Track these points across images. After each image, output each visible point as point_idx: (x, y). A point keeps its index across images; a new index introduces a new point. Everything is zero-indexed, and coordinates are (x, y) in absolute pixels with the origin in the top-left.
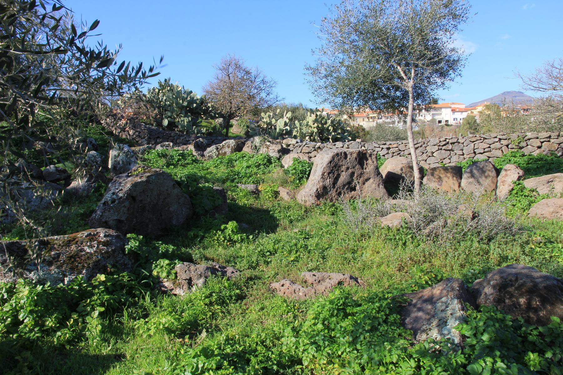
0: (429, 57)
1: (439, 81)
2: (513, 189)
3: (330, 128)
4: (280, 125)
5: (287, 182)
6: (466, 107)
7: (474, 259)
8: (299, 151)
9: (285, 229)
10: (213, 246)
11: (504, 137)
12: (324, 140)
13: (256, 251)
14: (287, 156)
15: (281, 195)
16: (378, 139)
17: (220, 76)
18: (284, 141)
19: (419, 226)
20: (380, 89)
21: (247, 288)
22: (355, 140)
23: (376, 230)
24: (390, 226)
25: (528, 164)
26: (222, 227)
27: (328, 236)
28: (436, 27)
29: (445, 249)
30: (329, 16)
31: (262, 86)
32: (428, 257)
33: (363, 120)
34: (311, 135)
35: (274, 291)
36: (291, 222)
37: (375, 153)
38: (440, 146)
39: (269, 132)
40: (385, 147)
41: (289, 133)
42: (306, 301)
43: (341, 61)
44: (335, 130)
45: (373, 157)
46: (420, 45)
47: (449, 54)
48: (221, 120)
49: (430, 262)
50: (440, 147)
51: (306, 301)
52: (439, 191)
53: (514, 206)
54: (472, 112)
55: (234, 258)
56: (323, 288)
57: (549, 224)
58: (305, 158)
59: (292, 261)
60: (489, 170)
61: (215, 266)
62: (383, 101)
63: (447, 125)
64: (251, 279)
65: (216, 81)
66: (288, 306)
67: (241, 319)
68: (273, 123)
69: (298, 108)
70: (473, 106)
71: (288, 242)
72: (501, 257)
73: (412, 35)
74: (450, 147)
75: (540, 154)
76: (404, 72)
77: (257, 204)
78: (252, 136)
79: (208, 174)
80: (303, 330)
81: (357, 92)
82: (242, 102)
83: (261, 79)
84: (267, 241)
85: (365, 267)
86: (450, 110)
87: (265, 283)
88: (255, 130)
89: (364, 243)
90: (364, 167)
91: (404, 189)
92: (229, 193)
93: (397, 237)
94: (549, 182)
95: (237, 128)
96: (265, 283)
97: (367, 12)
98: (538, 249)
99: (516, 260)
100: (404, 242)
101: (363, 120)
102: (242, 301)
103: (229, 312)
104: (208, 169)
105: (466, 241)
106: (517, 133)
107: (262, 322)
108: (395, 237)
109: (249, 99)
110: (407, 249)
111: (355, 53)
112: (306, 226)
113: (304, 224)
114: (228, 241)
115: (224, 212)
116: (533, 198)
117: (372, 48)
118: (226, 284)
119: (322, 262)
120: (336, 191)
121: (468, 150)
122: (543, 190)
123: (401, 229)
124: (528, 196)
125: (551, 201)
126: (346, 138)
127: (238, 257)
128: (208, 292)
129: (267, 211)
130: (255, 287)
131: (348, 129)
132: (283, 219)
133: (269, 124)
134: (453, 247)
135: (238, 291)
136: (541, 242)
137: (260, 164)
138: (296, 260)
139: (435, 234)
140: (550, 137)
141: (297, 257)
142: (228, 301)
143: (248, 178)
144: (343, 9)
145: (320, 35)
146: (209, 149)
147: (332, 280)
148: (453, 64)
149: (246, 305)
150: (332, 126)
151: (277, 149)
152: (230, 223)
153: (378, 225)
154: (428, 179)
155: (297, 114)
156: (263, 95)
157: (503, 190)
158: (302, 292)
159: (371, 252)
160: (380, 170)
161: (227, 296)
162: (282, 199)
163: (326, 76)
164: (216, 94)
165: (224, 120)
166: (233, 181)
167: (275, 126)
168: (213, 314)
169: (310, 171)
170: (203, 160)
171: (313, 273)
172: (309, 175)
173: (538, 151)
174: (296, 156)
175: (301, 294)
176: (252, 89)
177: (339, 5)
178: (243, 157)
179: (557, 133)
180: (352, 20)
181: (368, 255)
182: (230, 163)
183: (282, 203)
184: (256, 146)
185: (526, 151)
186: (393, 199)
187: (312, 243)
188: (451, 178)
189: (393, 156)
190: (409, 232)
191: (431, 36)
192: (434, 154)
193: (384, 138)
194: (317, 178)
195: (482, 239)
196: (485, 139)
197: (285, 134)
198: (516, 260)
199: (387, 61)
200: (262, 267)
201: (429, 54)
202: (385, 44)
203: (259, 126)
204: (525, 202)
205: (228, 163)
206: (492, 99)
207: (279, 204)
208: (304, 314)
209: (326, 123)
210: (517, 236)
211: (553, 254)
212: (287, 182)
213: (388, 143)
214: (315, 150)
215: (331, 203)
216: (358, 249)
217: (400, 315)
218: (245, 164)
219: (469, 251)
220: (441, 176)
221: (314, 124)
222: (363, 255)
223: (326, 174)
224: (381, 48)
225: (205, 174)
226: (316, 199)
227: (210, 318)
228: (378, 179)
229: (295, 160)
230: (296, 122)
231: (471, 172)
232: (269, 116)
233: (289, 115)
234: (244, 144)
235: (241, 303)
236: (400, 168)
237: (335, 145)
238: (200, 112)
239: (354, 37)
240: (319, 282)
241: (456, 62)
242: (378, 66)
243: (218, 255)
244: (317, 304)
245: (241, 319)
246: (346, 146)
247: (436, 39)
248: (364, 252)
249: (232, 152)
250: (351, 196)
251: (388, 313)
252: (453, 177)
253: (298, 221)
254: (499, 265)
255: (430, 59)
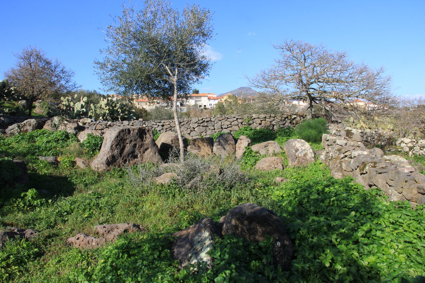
0: (187, 60)
1: (195, 78)
2: (245, 152)
3: (119, 110)
4: (78, 107)
5: (82, 153)
6: (217, 96)
7: (221, 202)
8: (94, 128)
9: (81, 191)
10: (12, 212)
11: (239, 117)
12: (115, 119)
13: (55, 213)
14: (82, 133)
15: (77, 164)
16: (156, 118)
17: (22, 64)
18: (81, 120)
19: (184, 182)
20: (154, 82)
21: (46, 246)
22: (138, 120)
23: (153, 187)
24: (163, 183)
25: (254, 135)
26: (22, 195)
27: (116, 194)
28: (191, 40)
29: (202, 197)
30: (113, 24)
31: (62, 75)
32: (191, 204)
33: (146, 104)
34: (104, 115)
35: (70, 245)
36: (86, 185)
37: (153, 129)
38: (199, 123)
39: (68, 114)
40: (160, 124)
41: (85, 114)
42: (98, 249)
43: (123, 59)
44: (123, 112)
45: (150, 132)
46: (181, 52)
47: (200, 59)
48: (24, 102)
49: (192, 207)
50: (199, 124)
51: (98, 249)
52: (199, 155)
53: (246, 163)
54: (221, 100)
55: (33, 221)
56: (113, 236)
57: (267, 174)
58: (97, 134)
59: (86, 217)
60: (230, 140)
61: (14, 230)
62: (156, 91)
63: (205, 109)
64: (49, 237)
65: (18, 68)
66: (82, 255)
67: (39, 274)
68: (71, 105)
69: (93, 94)
70: (221, 96)
71: (83, 202)
72: (238, 198)
73: (175, 44)
74: (206, 124)
75: (261, 128)
76: (171, 70)
77: (56, 173)
78: (53, 116)
79: (9, 148)
80: (95, 273)
81: (136, 84)
82: (44, 87)
83: (60, 69)
84: (64, 203)
85: (146, 216)
86: (206, 98)
87: (62, 239)
88: (55, 111)
89: (145, 198)
90: (144, 140)
91: (172, 155)
92: (30, 164)
93: (169, 191)
94: (265, 147)
95: (39, 109)
96: (62, 239)
97: (142, 24)
98: (260, 191)
99: (247, 200)
100: (173, 194)
101: (146, 104)
102: (41, 257)
103: (27, 270)
104: (9, 144)
105: (216, 190)
106: (247, 115)
107: (59, 273)
108: (165, 191)
109: (50, 85)
110: (175, 199)
111: (134, 54)
112: (99, 188)
113: (97, 186)
114: (28, 206)
115: (24, 181)
116: (257, 157)
117: (147, 51)
118: (25, 245)
119: (111, 216)
120: (123, 159)
121: (217, 126)
122: (263, 152)
123: (171, 185)
124: (254, 156)
125: (267, 159)
126: (132, 118)
127: (37, 220)
128: (5, 255)
129: (65, 178)
130: (53, 243)
131: (133, 111)
132: (79, 183)
133: (68, 106)
134: (207, 195)
135: (36, 250)
136: (262, 186)
137: (59, 139)
138: (90, 216)
139: (195, 187)
140: (265, 117)
141: (90, 214)
142: (26, 260)
143: (48, 151)
144: (124, 20)
145: (107, 38)
146: (10, 127)
147: (119, 229)
148: (204, 67)
149: (44, 260)
150: (120, 109)
151: (73, 127)
152: (30, 191)
153: (154, 183)
154: (191, 148)
155: (92, 98)
156: (63, 82)
157: (239, 153)
158: (94, 242)
159: (149, 204)
160: (156, 142)
161: (25, 256)
162: (79, 167)
163: (112, 70)
164: (19, 80)
165: (27, 102)
166: (33, 154)
167: (73, 108)
168: (10, 275)
169: (101, 144)
170: (5, 136)
171: (103, 226)
172: (100, 147)
173: (260, 127)
174: (90, 132)
175: (94, 244)
176: (53, 77)
177: (121, 17)
178: (44, 134)
179: (269, 115)
180: (131, 29)
181: (147, 207)
182: (32, 138)
183: (79, 171)
184: (55, 124)
185: (253, 126)
186: (165, 163)
187: (103, 200)
188: (206, 146)
189: (166, 131)
190: (177, 185)
191: (189, 46)
192: (195, 129)
193: (160, 117)
194: (107, 149)
195: (226, 188)
196: (228, 118)
197: (82, 115)
198: (247, 200)
199: (158, 61)
200: (60, 226)
201: (188, 59)
202: (156, 49)
203: (59, 108)
204: (253, 160)
205: (29, 139)
206: (231, 92)
207: (75, 172)
208: (96, 260)
209: (116, 106)
210: (248, 184)
211: (269, 194)
212: (82, 153)
213: (162, 121)
214: (107, 127)
215: (119, 169)
216: (139, 203)
217: (169, 250)
218: (45, 140)
219: (218, 196)
220: (200, 145)
221: (106, 107)
222: (144, 207)
223: (114, 146)
224: (154, 52)
225: (7, 149)
226: (107, 166)
227: (6, 279)
228: (154, 149)
229: (89, 135)
230: (92, 105)
231: (219, 142)
232: (68, 100)
233: (85, 99)
234: (44, 123)
235: (39, 260)
236: (171, 140)
237: (122, 123)
238: (2, 94)
239: (133, 42)
240: (109, 232)
241: (205, 66)
242: (151, 65)
243: (17, 220)
244: (106, 251)
245: (39, 274)
246: (131, 124)
247: (192, 48)
248: (144, 204)
249: (33, 130)
250: (134, 162)
251: (161, 249)
252: (208, 145)
253: (92, 184)
254: (237, 204)
255: (188, 62)
